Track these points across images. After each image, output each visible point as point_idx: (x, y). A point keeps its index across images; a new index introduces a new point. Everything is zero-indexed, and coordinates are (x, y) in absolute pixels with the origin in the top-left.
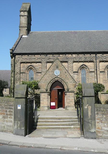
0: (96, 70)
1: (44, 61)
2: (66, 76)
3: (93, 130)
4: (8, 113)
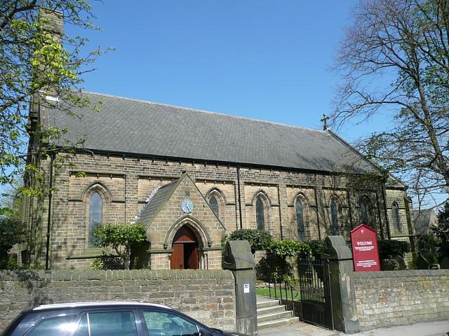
0: (239, 201)
1: (132, 174)
2: (205, 214)
3: (355, 319)
4: (223, 304)
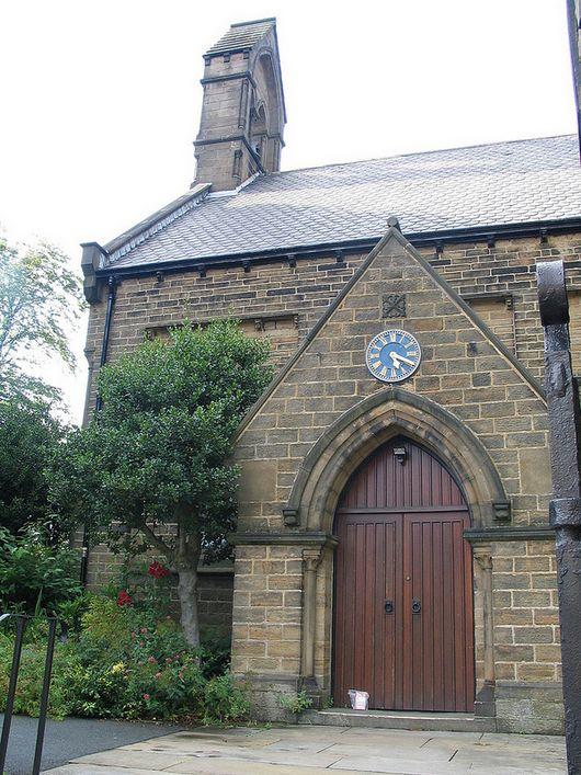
2: (478, 380)
